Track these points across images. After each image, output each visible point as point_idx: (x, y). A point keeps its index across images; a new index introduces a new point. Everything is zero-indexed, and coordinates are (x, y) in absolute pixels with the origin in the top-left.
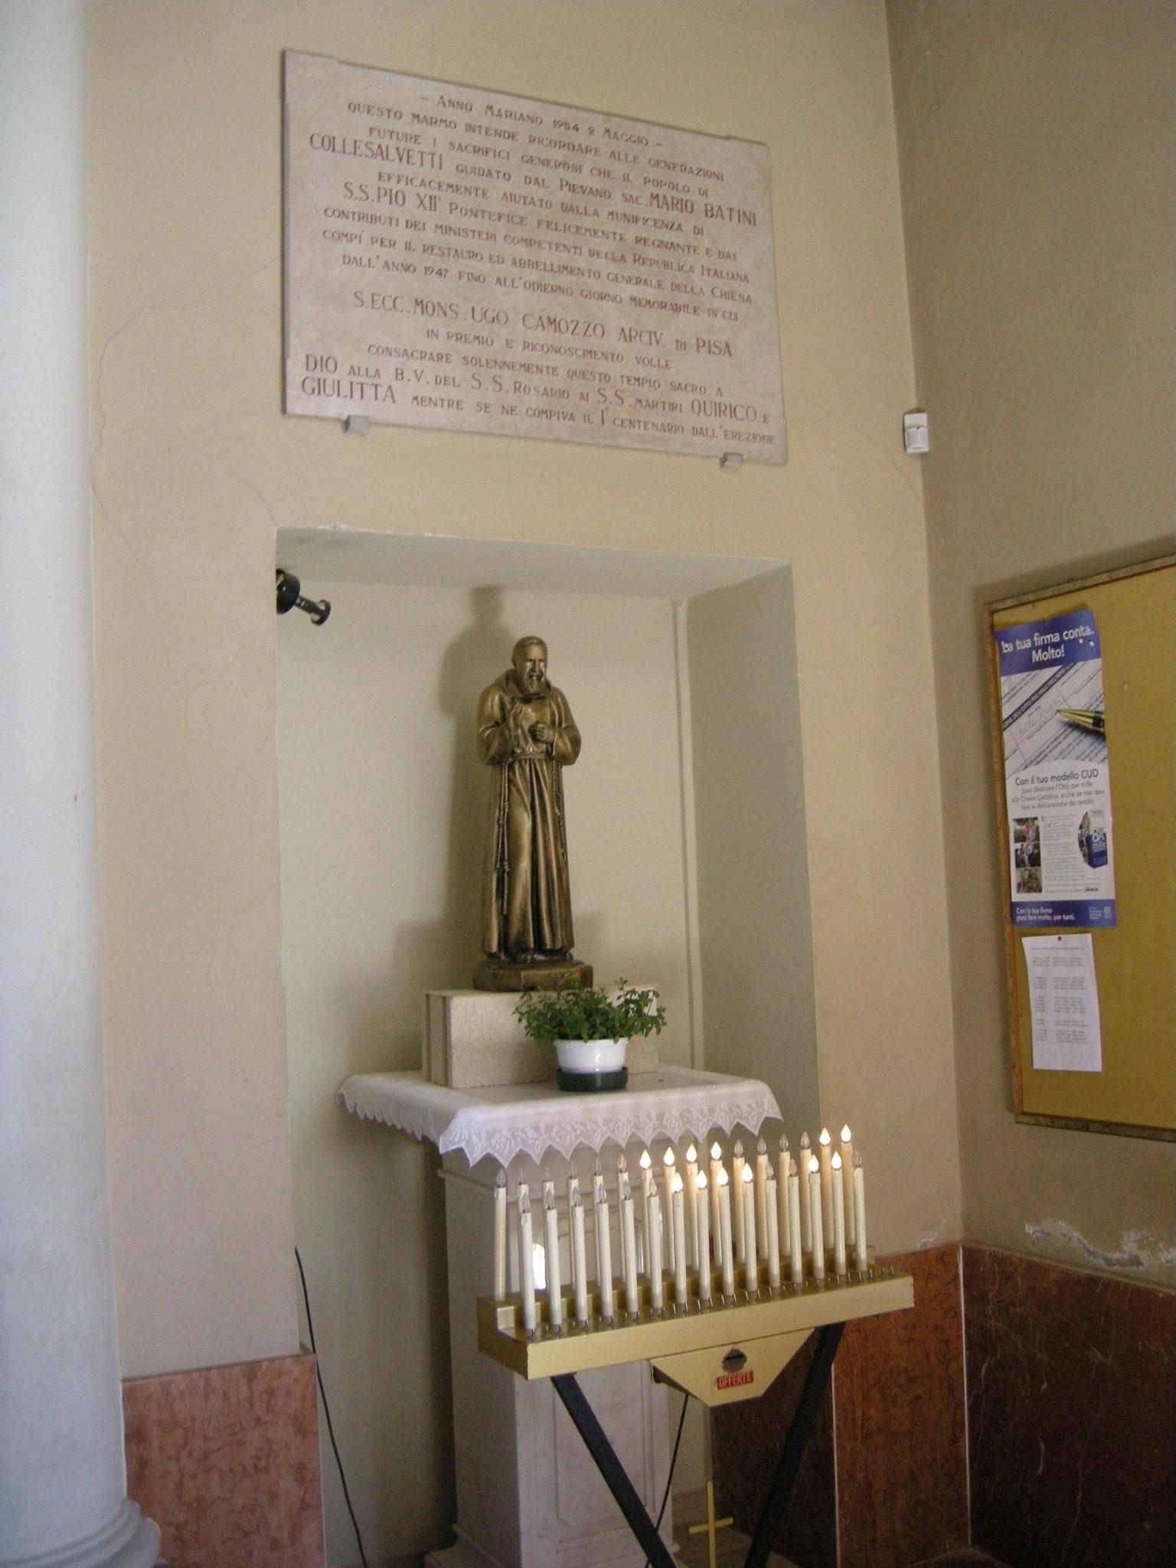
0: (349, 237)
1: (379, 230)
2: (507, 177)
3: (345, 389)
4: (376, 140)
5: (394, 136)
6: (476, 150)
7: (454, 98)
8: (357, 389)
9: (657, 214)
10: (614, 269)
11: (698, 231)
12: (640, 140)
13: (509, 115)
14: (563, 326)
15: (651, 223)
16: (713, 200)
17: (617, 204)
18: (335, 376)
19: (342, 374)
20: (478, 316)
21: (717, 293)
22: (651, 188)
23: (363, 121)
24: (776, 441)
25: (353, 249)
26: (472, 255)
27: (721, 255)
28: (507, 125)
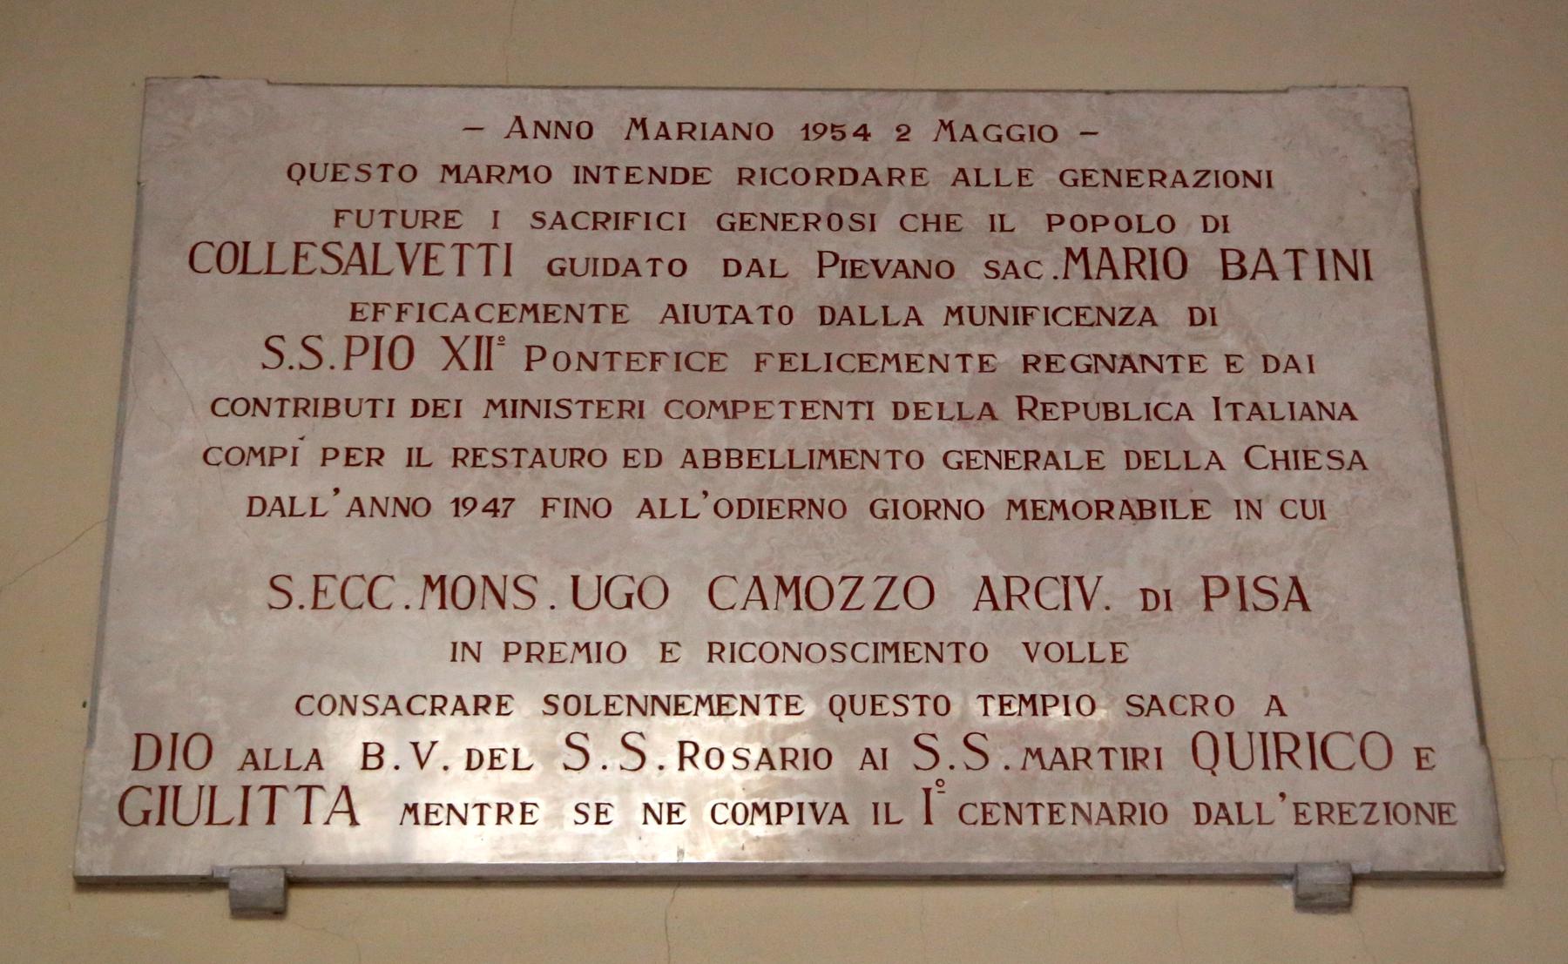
0: (265, 456)
1: (342, 431)
2: (678, 268)
3: (229, 805)
4: (349, 234)
5: (395, 220)
6: (600, 221)
7: (548, 115)
8: (259, 801)
9: (1080, 292)
10: (960, 438)
11: (1201, 317)
12: (1035, 133)
13: (687, 130)
14: (819, 593)
15: (1064, 317)
16: (1243, 237)
17: (974, 288)
18: (205, 778)
19: (226, 773)
20: (587, 598)
21: (1262, 457)
22: (1068, 237)
23: (323, 196)
24: (1458, 814)
25: (274, 481)
26: (578, 456)
27: (1269, 363)
28: (683, 154)
